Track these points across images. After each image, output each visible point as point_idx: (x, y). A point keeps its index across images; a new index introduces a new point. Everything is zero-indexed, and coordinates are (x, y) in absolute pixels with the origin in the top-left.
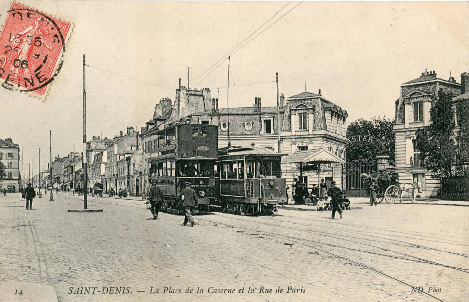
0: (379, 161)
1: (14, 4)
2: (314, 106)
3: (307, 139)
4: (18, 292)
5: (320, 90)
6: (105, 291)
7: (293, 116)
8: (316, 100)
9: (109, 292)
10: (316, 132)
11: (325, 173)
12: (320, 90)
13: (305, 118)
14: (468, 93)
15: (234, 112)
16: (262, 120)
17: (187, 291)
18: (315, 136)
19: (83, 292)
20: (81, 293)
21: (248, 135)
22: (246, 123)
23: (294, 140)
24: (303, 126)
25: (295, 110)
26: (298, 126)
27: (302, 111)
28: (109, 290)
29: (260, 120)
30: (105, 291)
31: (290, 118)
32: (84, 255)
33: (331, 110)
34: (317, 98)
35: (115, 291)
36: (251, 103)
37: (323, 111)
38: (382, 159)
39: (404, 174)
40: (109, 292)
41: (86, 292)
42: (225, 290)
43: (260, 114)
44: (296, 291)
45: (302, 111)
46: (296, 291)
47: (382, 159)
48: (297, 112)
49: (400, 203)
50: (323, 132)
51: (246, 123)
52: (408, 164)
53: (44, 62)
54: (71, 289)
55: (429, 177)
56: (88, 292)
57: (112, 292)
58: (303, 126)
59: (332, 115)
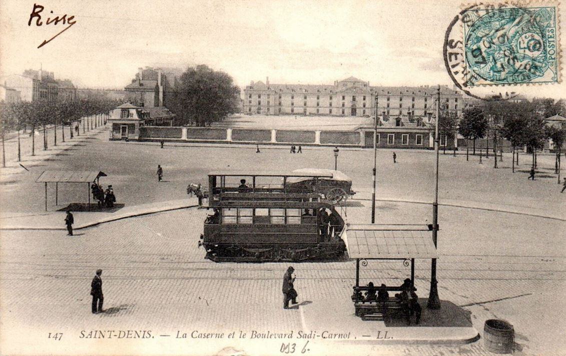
4: (51, 336)
5: (38, 48)
6: (122, 334)
9: (126, 336)
12: (38, 48)
14: (565, 157)
19: (97, 336)
20: (143, 337)
28: (126, 335)
30: (122, 334)
35: (133, 335)
40: (126, 336)
41: (101, 336)
42: (335, 335)
44: (283, 336)
46: (283, 336)
49: (122, 139)
53: (41, 182)
54: (83, 333)
56: (103, 337)
57: (129, 336)
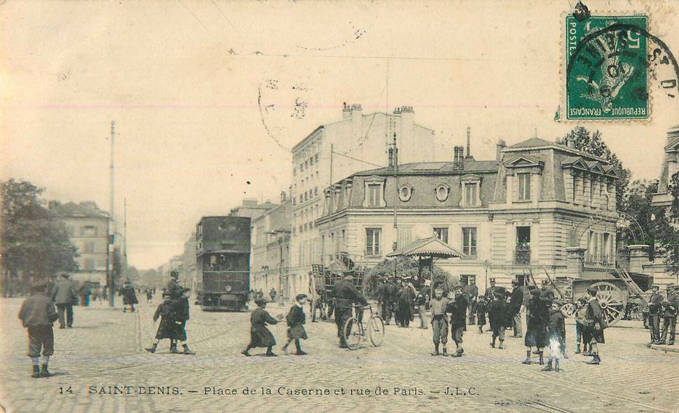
0: (632, 252)
1: (581, 16)
2: (543, 163)
3: (530, 215)
7: (509, 178)
8: (546, 153)
10: (544, 205)
11: (557, 270)
13: (528, 182)
15: (410, 170)
16: (463, 183)
17: (246, 391)
18: (541, 212)
21: (440, 207)
22: (438, 189)
23: (510, 217)
24: (526, 195)
25: (514, 168)
26: (517, 194)
27: (523, 171)
29: (461, 184)
31: (505, 180)
32: (112, 338)
33: (571, 168)
34: (548, 149)
36: (450, 157)
37: (558, 170)
38: (636, 250)
39: (503, 275)
43: (461, 174)
45: (523, 171)
47: (636, 250)
48: (516, 171)
50: (554, 205)
51: (438, 189)
52: (509, 262)
55: (661, 287)
58: (526, 195)
59: (575, 177)
